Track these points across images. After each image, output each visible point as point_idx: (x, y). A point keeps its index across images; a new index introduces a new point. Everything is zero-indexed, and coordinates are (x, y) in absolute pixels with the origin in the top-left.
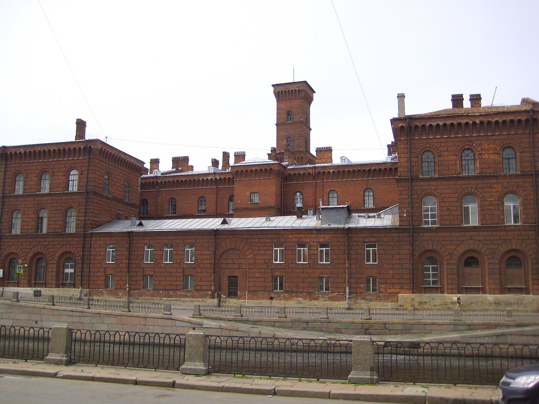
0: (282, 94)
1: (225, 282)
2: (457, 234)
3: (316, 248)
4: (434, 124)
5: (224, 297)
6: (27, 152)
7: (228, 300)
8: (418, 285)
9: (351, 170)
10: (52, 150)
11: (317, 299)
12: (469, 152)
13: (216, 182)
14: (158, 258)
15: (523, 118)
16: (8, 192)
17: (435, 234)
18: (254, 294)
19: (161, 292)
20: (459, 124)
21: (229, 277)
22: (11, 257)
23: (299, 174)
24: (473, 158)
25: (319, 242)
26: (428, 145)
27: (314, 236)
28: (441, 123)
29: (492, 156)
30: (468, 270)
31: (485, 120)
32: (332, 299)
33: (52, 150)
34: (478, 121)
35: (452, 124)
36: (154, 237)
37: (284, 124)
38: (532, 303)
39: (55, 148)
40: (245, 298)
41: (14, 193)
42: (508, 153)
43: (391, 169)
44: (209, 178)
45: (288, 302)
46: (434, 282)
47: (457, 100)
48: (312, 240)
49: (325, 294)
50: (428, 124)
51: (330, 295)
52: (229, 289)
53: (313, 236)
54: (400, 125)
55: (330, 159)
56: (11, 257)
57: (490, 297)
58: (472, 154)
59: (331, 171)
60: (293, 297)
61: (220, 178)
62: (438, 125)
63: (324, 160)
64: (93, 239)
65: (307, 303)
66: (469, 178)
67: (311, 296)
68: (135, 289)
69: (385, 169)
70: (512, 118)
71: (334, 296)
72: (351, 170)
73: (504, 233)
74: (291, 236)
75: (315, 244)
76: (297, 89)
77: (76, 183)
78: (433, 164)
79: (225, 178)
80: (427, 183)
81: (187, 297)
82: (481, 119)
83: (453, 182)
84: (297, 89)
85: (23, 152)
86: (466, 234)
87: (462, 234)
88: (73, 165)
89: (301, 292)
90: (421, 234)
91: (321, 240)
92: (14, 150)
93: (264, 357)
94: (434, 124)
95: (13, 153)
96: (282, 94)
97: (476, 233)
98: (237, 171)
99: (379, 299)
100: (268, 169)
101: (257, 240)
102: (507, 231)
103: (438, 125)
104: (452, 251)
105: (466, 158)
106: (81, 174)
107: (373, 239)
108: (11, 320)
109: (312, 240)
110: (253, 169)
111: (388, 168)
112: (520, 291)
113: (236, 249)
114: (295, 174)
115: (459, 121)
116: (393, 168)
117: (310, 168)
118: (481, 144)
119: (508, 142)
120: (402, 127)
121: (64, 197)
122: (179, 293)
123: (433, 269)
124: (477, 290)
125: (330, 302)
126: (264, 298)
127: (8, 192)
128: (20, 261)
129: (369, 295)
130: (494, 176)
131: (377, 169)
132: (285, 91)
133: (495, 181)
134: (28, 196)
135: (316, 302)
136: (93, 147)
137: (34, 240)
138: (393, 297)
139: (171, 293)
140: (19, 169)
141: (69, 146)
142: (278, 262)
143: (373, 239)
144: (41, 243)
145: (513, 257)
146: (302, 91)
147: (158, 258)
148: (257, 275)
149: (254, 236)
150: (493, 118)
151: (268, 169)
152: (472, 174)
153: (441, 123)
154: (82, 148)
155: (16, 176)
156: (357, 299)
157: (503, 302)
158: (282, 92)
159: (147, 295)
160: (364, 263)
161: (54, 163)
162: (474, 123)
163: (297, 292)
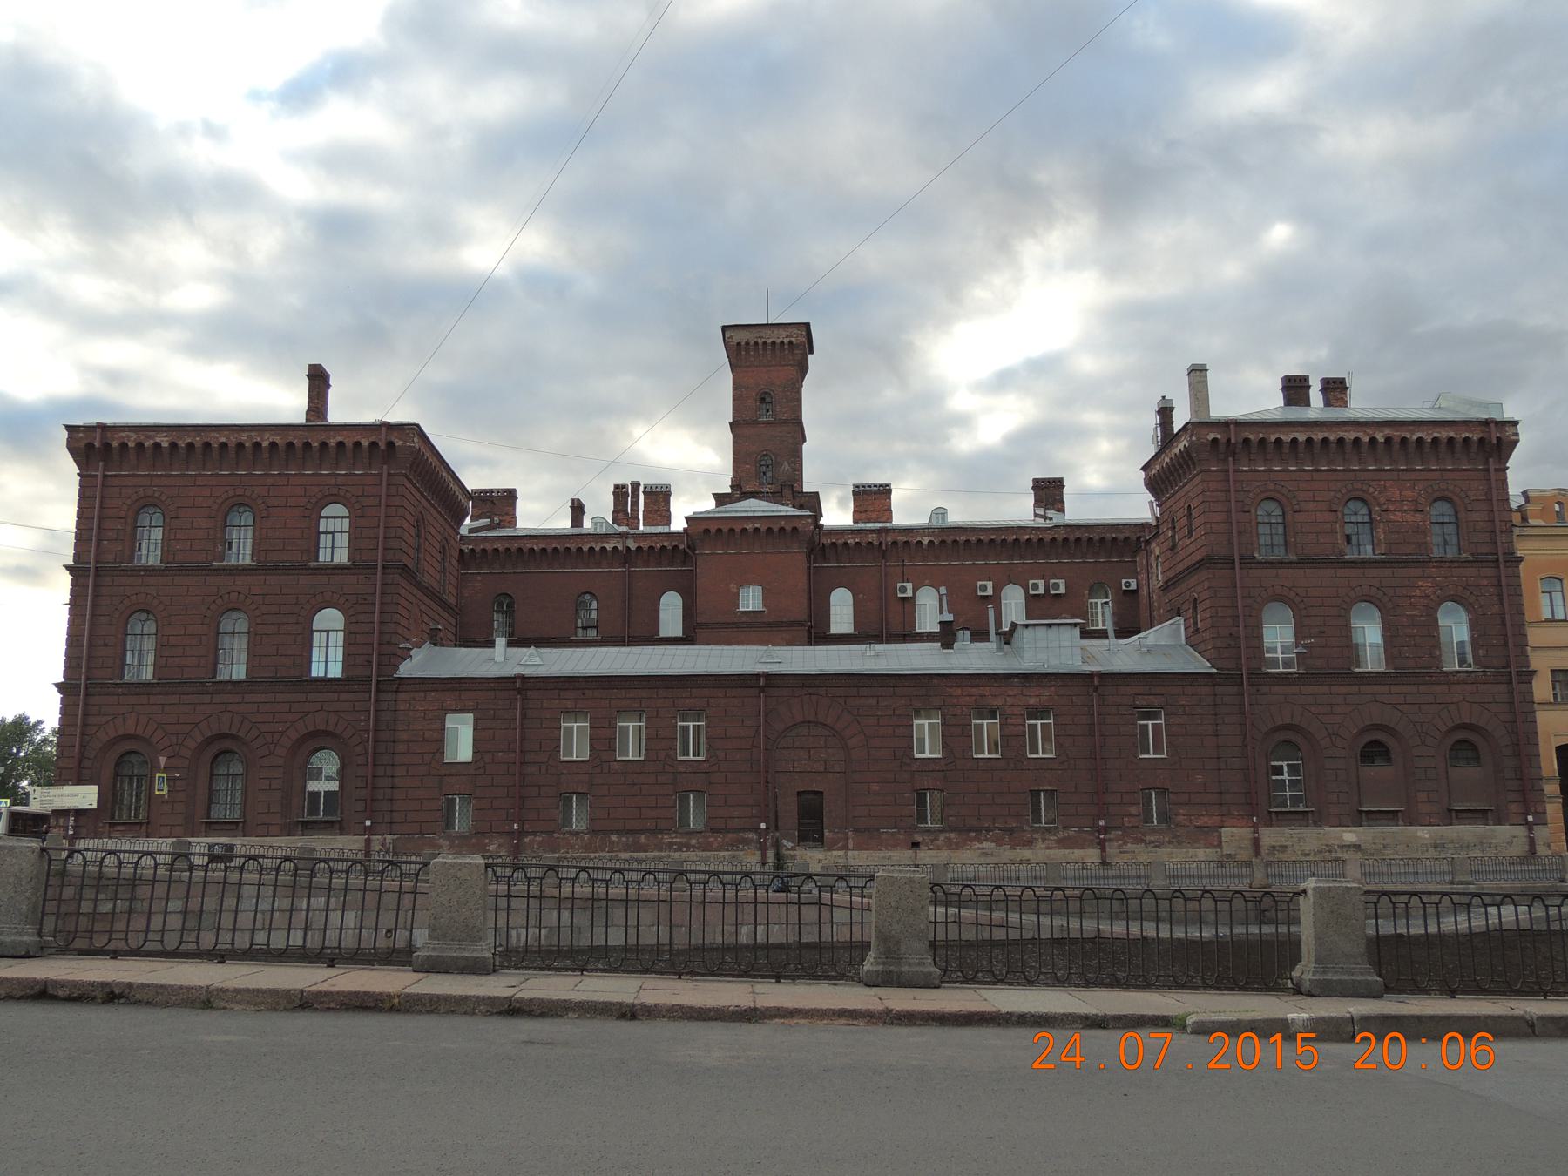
0: (747, 350)
1: (789, 808)
2: (1343, 690)
3: (1019, 721)
4: (1287, 438)
5: (790, 845)
6: (181, 444)
7: (799, 852)
8: (1261, 808)
9: (973, 539)
10: (265, 444)
11: (1029, 844)
12: (1359, 504)
13: (626, 557)
14: (603, 742)
15: (1475, 436)
16: (110, 557)
17: (1295, 689)
18: (869, 835)
19: (614, 838)
20: (1341, 441)
21: (799, 793)
22: (227, 745)
23: (846, 544)
24: (1366, 519)
25: (1027, 707)
26: (1271, 486)
27: (1016, 691)
28: (1302, 438)
29: (1409, 517)
30: (1372, 771)
31: (1397, 434)
32: (1064, 843)
33: (265, 444)
34: (1380, 437)
35: (1325, 441)
36: (589, 693)
37: (747, 423)
38: (1510, 844)
39: (277, 439)
40: (846, 848)
41: (131, 561)
42: (1441, 510)
43: (1066, 540)
44: (609, 546)
45: (958, 853)
46: (1295, 800)
47: (1295, 389)
48: (1010, 701)
49: (1048, 830)
50: (1273, 438)
51: (1060, 835)
52: (800, 824)
53: (1011, 691)
54: (1211, 436)
55: (887, 512)
56: (227, 745)
57: (1424, 833)
58: (1365, 511)
59: (926, 541)
60: (971, 840)
61: (639, 548)
62: (1294, 440)
63: (874, 515)
64: (402, 696)
65: (1006, 854)
66: (1363, 563)
67: (1013, 836)
68: (534, 833)
69: (1054, 540)
70: (1452, 434)
71: (1069, 838)
72: (973, 539)
73: (1444, 688)
74: (959, 691)
75: (1017, 711)
76: (786, 341)
77: (343, 540)
78: (1280, 529)
79: (651, 548)
80: (1272, 572)
81: (689, 847)
82: (1388, 431)
83: (1329, 572)
84: (786, 341)
85: (165, 444)
86: (1364, 689)
87: (1354, 689)
88: (335, 491)
89: (988, 830)
90: (1265, 689)
91: (1032, 701)
92: (134, 436)
93: (772, 994)
94: (1287, 438)
95: (131, 444)
96: (747, 350)
97: (1385, 689)
98: (707, 531)
99: (1177, 842)
100: (788, 528)
101: (872, 701)
102: (1448, 683)
103: (1294, 440)
104: (277, 736)
105: (1353, 519)
106: (355, 518)
107: (1156, 701)
108: (202, 934)
109: (1010, 701)
110: (749, 527)
111: (1060, 539)
112: (1480, 816)
113: (817, 723)
114: (834, 544)
115: (1341, 435)
116: (1072, 538)
117: (872, 531)
118: (1386, 489)
119: (1443, 485)
120: (1215, 440)
121: (303, 580)
122: (667, 839)
123: (1293, 770)
124: (1392, 817)
125: (1062, 851)
126: (894, 846)
127: (110, 557)
128: (162, 760)
129: (1154, 831)
130: (1417, 561)
131: (1035, 540)
132: (756, 343)
133: (1418, 572)
134: (183, 570)
135: (1027, 853)
136: (399, 443)
137: (207, 698)
138: (1207, 834)
139: (643, 839)
140: (149, 492)
141: (322, 437)
142: (926, 755)
143: (1156, 701)
144: (230, 708)
145: (1287, 742)
146: (798, 346)
147: (603, 742)
148: (875, 787)
149: (864, 691)
150: (1412, 432)
151: (788, 528)
152: (1368, 552)
153: (1302, 438)
154: (365, 443)
155: (138, 513)
156: (1125, 843)
157: (1452, 842)
158: (747, 343)
159: (572, 847)
160: (557, 759)
161: (270, 481)
162: (1373, 440)
163: (978, 830)
